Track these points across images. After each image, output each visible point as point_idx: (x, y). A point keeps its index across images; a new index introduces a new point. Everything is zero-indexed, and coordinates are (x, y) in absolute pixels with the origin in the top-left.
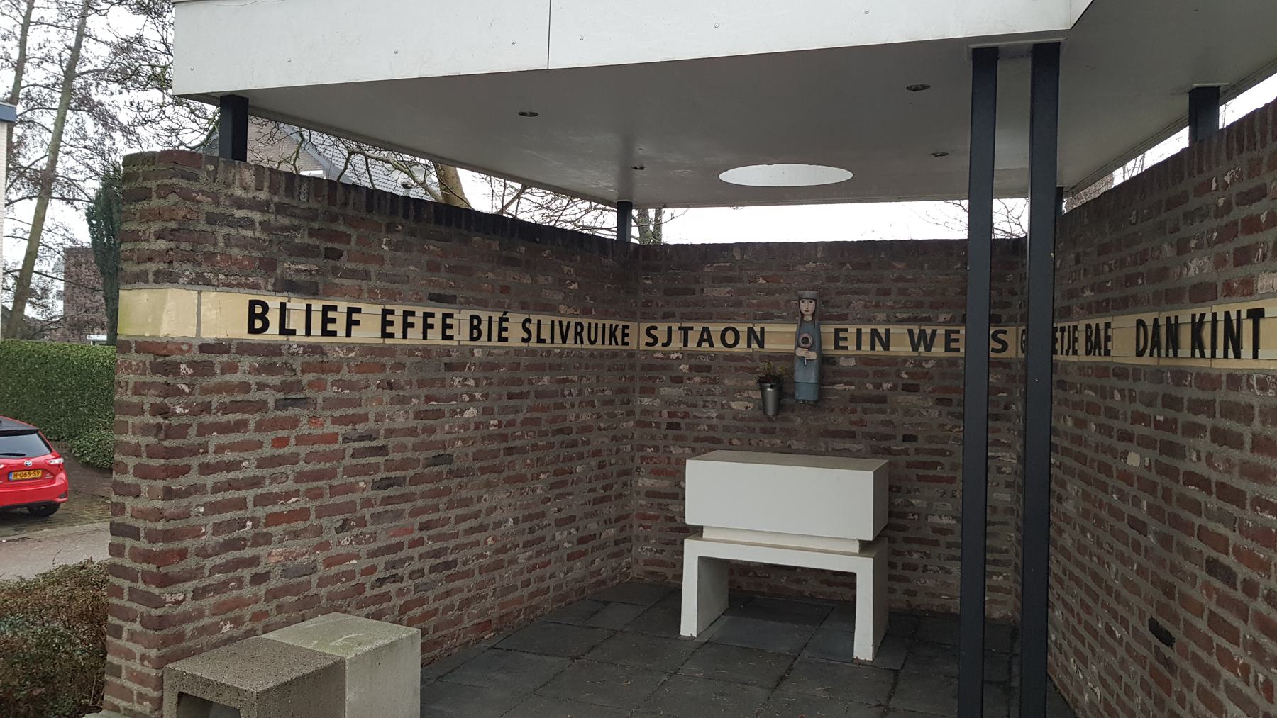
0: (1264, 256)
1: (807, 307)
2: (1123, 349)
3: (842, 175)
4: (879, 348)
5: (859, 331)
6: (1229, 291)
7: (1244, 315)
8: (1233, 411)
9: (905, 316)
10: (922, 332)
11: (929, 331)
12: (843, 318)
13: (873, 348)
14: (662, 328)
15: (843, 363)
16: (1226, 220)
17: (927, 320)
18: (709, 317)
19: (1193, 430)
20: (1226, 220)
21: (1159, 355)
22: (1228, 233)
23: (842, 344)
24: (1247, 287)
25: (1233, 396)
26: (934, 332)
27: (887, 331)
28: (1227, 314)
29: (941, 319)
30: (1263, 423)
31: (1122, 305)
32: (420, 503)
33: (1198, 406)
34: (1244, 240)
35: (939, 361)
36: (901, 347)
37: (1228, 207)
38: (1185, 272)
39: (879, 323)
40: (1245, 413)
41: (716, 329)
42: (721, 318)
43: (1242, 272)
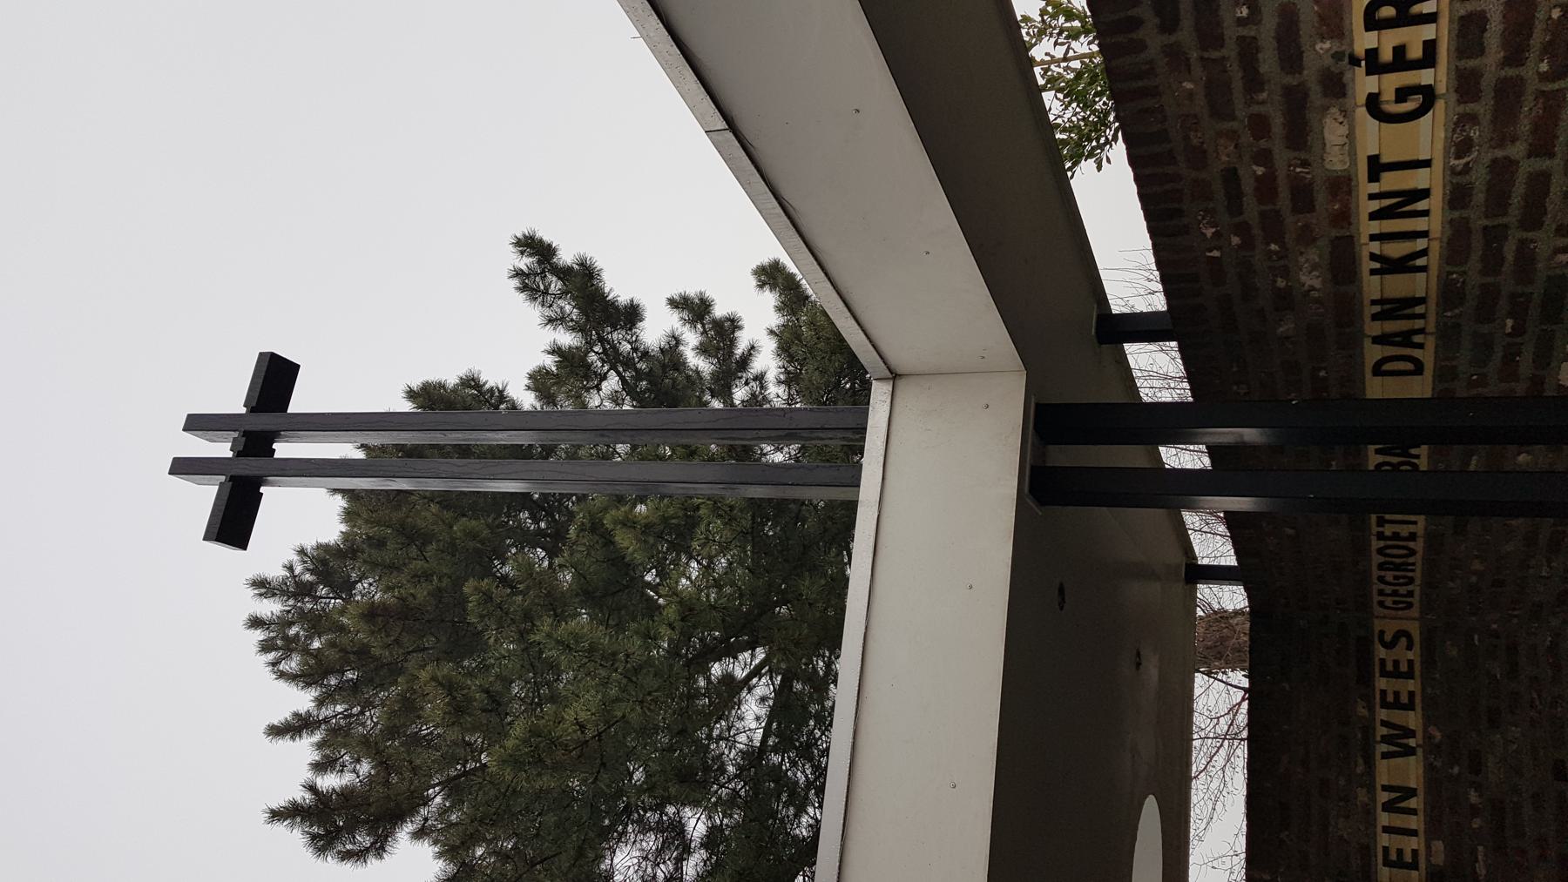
0: (1305, 164)
3: (1151, 806)
4: (1413, 803)
5: (1386, 830)
6: (1344, 217)
7: (1374, 188)
8: (1498, 200)
9: (1360, 761)
10: (1386, 739)
11: (1384, 731)
12: (1366, 851)
13: (1414, 812)
15: (1439, 859)
16: (1257, 231)
17: (1368, 730)
19: (1526, 257)
20: (1257, 231)
21: (1422, 331)
22: (1273, 226)
23: (1408, 858)
24: (1342, 185)
25: (1479, 197)
26: (1384, 723)
27: (1385, 788)
28: (1374, 216)
29: (1364, 712)
30: (1514, 140)
33: (1493, 262)
34: (1284, 200)
35: (1428, 720)
36: (1411, 771)
37: (1243, 229)
38: (1315, 294)
39: (1374, 800)
40: (1502, 170)
43: (1321, 197)
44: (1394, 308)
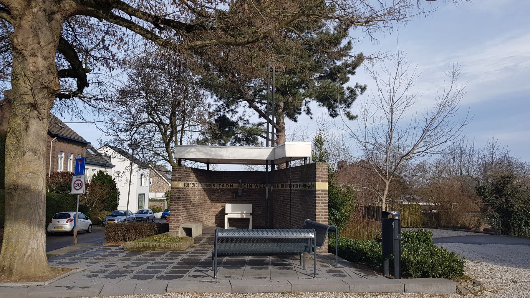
1: (240, 181)
2: (280, 187)
14: (216, 184)
18: (224, 183)
31: (280, 183)
32: (324, 179)
36: (253, 187)
41: (225, 184)
42: (226, 183)
44: (278, 187)
